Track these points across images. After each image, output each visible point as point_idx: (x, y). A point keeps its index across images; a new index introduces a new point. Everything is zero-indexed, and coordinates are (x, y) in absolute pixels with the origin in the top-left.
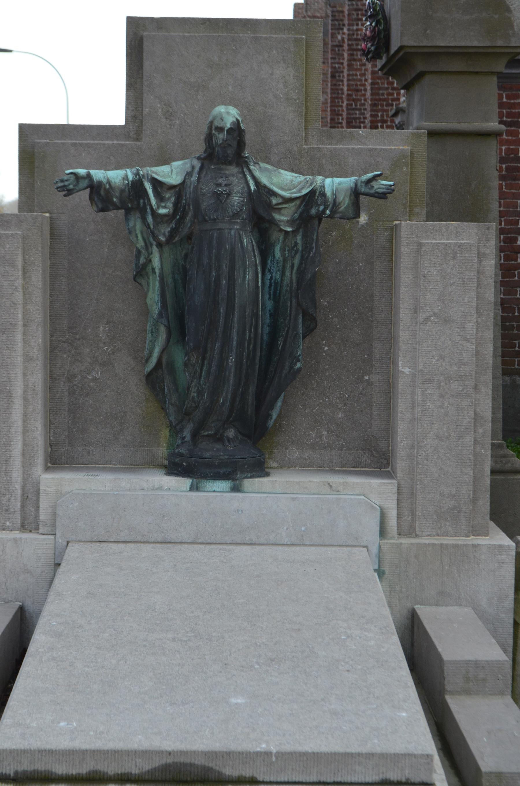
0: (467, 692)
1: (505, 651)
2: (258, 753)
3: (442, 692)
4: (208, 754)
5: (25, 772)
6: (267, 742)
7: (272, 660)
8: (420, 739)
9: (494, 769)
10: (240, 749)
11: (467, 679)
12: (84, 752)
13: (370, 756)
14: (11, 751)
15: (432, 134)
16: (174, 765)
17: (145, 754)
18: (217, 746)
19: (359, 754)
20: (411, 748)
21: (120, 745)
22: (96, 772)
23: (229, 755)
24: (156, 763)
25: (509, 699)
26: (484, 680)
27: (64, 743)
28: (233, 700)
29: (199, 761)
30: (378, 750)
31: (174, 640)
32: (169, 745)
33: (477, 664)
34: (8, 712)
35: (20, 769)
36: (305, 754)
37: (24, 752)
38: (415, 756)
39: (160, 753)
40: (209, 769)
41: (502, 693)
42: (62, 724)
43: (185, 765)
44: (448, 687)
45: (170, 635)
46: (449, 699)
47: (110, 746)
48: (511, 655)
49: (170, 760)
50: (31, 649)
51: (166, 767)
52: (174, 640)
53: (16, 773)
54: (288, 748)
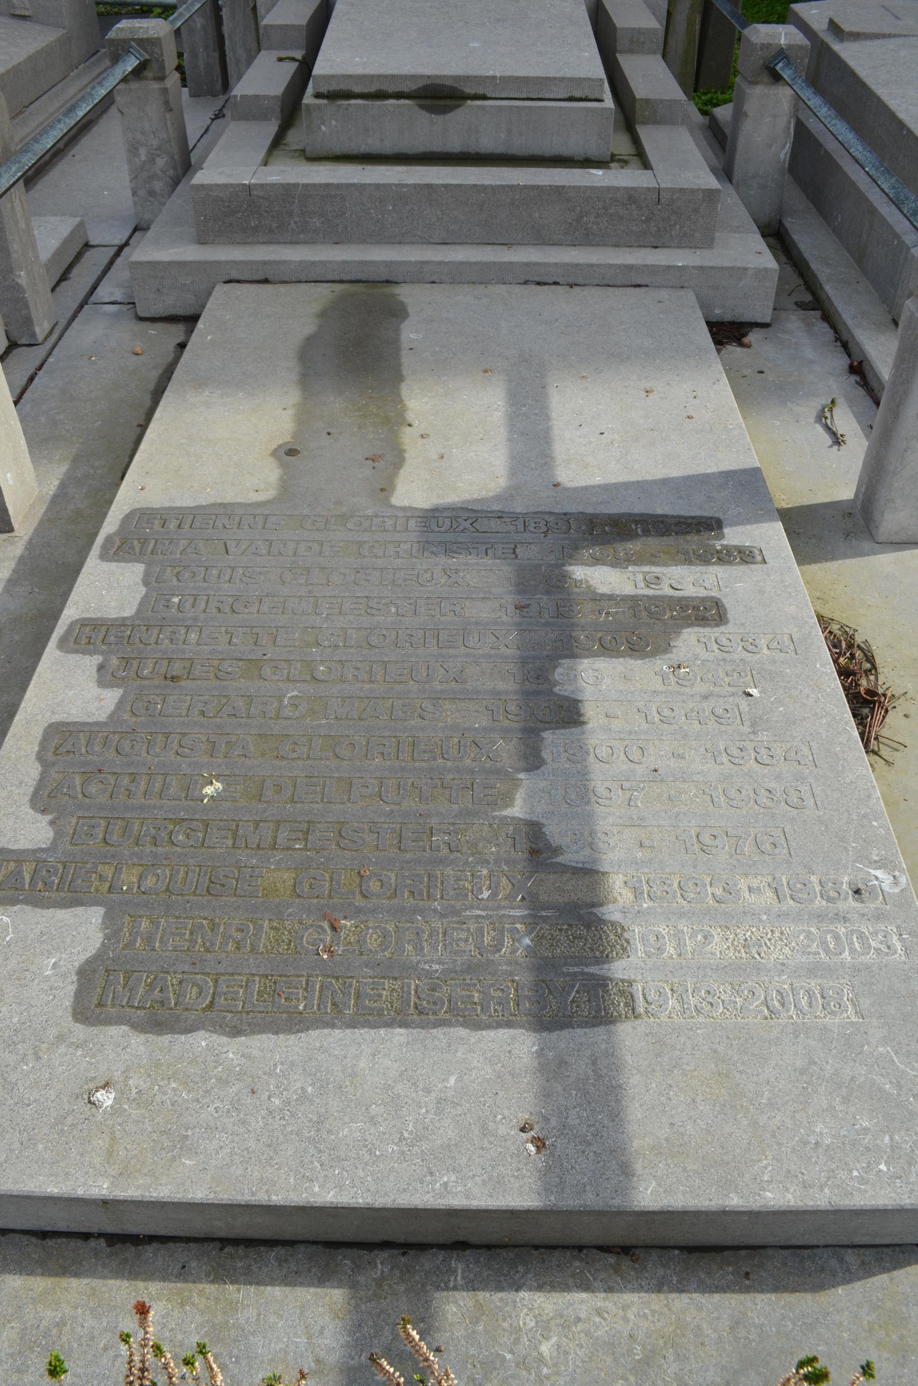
0: (631, 51)
1: (661, 24)
2: (488, 77)
3: (614, 51)
4: (458, 78)
5: (334, 91)
6: (494, 70)
7: (499, 20)
8: (598, 71)
9: (644, 97)
10: (475, 74)
11: (632, 42)
12: (372, 76)
13: (562, 79)
14: (324, 76)
15: (602, 101)
16: (432, 85)
17: (413, 78)
18: (460, 72)
19: (555, 78)
20: (590, 75)
21: (395, 72)
22: (380, 91)
23: (467, 78)
24: (420, 84)
25: (659, 57)
26: (643, 42)
27: (359, 71)
28: (471, 45)
29: (449, 83)
30: (568, 75)
31: (431, 7)
32: (428, 72)
33: (639, 31)
34: (9, 740)
35: (331, 89)
36: (519, 78)
37: (333, 76)
38: (592, 80)
39: (422, 77)
40: (455, 89)
41: (654, 52)
42: (357, 59)
43: (439, 85)
44: (618, 48)
45: (429, 4)
46: (618, 56)
47: (390, 72)
48: (664, 23)
49: (429, 82)
50: (334, 14)
51: (426, 88)
52: (431, 7)
53: (328, 91)
54: (507, 74)
